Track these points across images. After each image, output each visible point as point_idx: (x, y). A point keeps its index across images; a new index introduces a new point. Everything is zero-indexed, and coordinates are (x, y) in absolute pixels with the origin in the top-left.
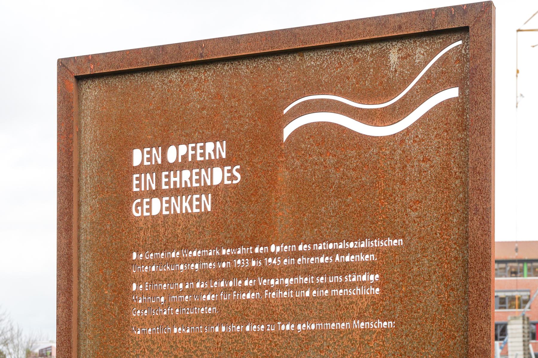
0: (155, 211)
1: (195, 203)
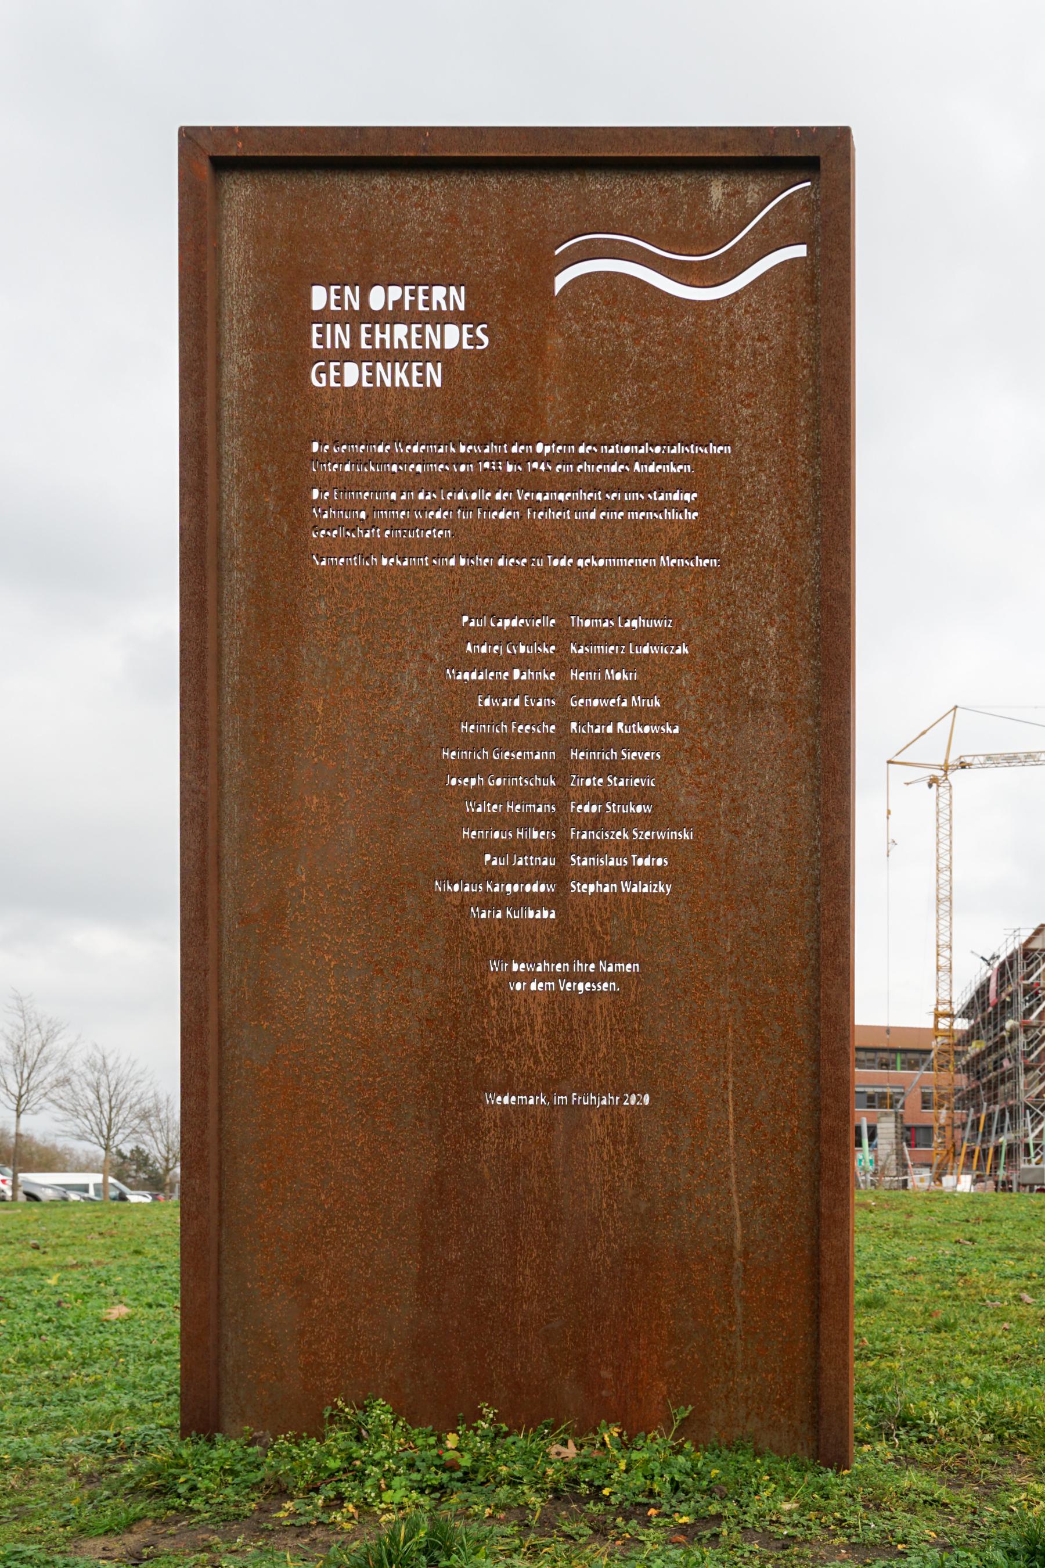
0: (350, 381)
1: (415, 374)
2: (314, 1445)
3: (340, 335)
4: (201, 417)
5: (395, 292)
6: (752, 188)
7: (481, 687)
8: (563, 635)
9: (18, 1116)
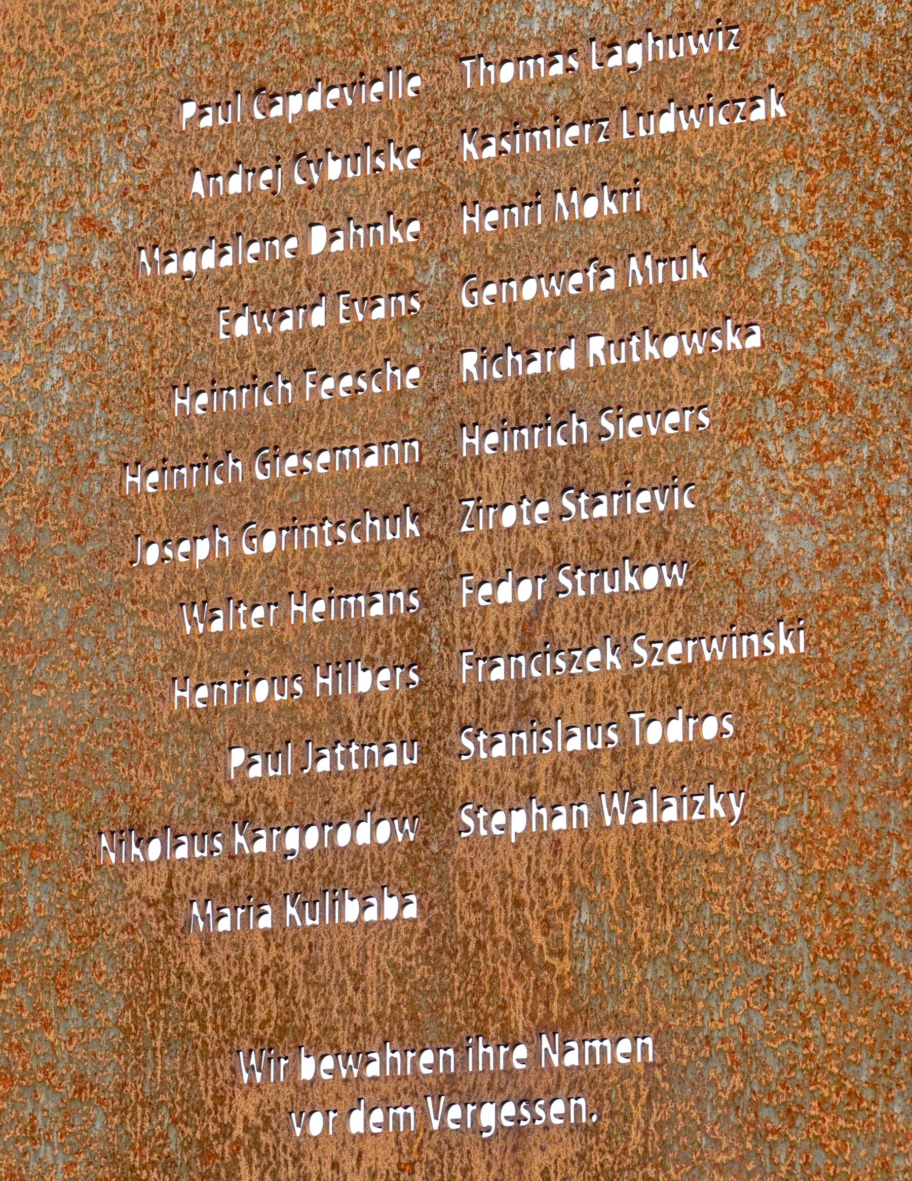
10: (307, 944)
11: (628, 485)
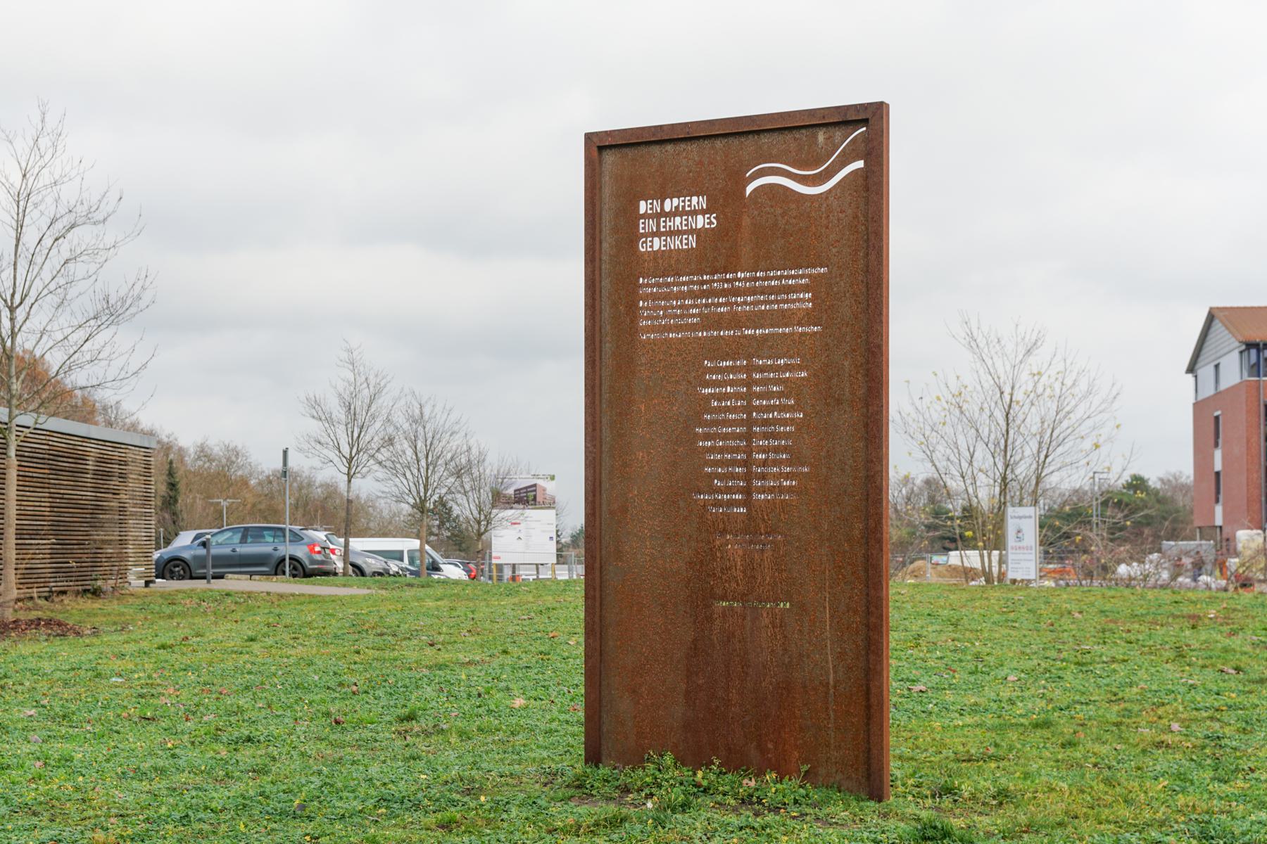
2: (640, 772)
3: (652, 225)
4: (593, 272)
5: (675, 201)
6: (838, 134)
7: (712, 396)
8: (749, 369)
9: (349, 481)
10: (728, 515)
11: (781, 439)
